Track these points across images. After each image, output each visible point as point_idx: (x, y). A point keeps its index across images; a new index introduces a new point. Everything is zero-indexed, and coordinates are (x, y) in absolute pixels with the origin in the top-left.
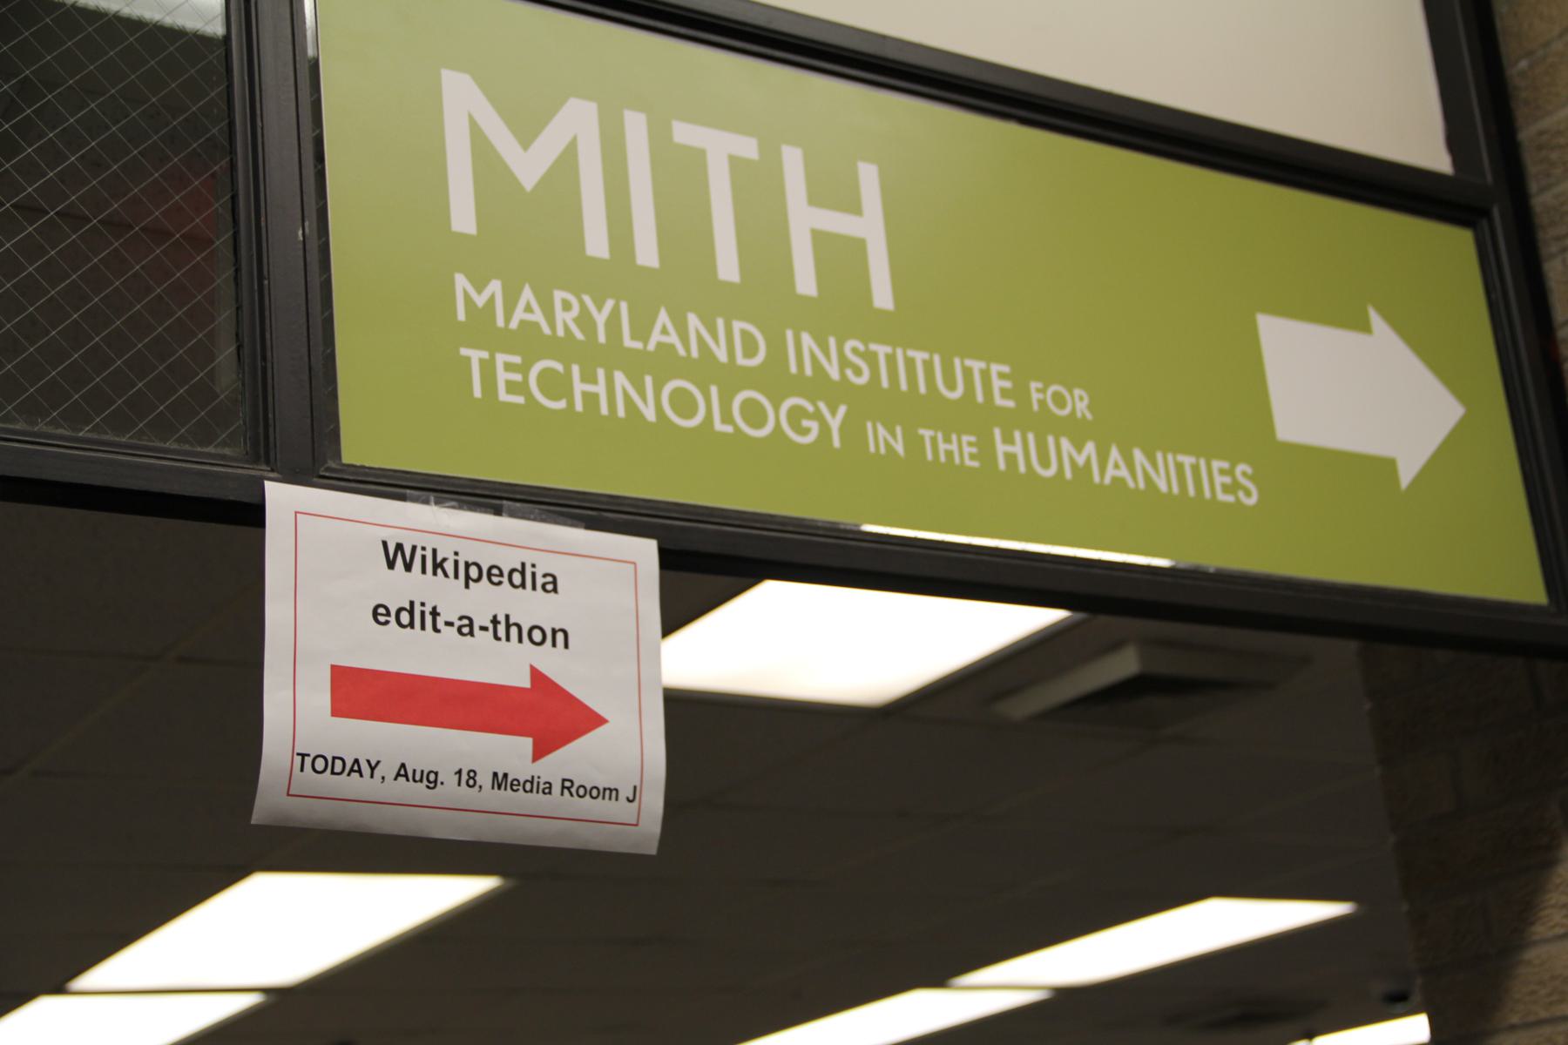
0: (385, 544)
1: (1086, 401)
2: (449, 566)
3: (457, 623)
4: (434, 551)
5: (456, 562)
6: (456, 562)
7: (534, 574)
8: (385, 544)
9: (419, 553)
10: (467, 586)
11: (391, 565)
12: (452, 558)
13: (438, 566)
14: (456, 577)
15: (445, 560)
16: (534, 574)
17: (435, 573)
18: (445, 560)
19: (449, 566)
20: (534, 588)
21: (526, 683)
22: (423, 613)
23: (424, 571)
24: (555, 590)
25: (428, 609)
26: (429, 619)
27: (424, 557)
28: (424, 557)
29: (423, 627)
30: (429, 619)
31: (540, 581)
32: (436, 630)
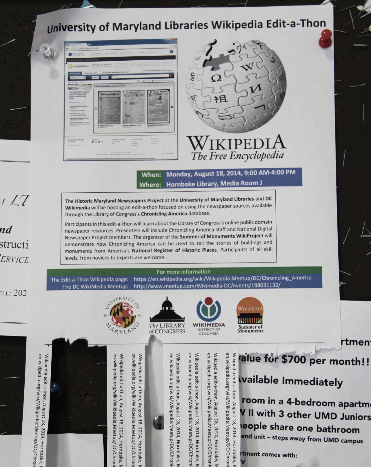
0: (212, 22)
1: (46, 45)
2: (231, 25)
3: (291, 24)
4: (227, 21)
5: (233, 24)
6: (233, 24)
7: (256, 23)
8: (212, 22)
9: (222, 23)
10: (236, 30)
11: (214, 27)
12: (232, 23)
13: (228, 26)
14: (233, 28)
15: (230, 24)
16: (256, 23)
17: (227, 28)
18: (230, 24)
19: (231, 25)
20: (256, 27)
21: (220, 66)
22: (280, 23)
23: (224, 28)
24: (262, 27)
25: (282, 21)
26: (282, 24)
27: (224, 24)
28: (224, 24)
29: (280, 26)
30: (282, 24)
31: (257, 25)
32: (284, 27)
